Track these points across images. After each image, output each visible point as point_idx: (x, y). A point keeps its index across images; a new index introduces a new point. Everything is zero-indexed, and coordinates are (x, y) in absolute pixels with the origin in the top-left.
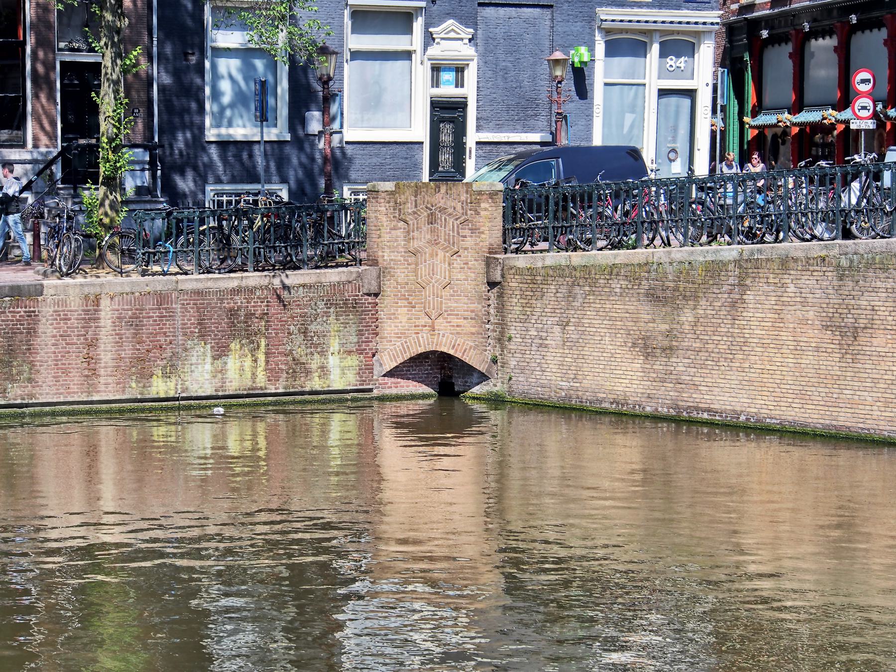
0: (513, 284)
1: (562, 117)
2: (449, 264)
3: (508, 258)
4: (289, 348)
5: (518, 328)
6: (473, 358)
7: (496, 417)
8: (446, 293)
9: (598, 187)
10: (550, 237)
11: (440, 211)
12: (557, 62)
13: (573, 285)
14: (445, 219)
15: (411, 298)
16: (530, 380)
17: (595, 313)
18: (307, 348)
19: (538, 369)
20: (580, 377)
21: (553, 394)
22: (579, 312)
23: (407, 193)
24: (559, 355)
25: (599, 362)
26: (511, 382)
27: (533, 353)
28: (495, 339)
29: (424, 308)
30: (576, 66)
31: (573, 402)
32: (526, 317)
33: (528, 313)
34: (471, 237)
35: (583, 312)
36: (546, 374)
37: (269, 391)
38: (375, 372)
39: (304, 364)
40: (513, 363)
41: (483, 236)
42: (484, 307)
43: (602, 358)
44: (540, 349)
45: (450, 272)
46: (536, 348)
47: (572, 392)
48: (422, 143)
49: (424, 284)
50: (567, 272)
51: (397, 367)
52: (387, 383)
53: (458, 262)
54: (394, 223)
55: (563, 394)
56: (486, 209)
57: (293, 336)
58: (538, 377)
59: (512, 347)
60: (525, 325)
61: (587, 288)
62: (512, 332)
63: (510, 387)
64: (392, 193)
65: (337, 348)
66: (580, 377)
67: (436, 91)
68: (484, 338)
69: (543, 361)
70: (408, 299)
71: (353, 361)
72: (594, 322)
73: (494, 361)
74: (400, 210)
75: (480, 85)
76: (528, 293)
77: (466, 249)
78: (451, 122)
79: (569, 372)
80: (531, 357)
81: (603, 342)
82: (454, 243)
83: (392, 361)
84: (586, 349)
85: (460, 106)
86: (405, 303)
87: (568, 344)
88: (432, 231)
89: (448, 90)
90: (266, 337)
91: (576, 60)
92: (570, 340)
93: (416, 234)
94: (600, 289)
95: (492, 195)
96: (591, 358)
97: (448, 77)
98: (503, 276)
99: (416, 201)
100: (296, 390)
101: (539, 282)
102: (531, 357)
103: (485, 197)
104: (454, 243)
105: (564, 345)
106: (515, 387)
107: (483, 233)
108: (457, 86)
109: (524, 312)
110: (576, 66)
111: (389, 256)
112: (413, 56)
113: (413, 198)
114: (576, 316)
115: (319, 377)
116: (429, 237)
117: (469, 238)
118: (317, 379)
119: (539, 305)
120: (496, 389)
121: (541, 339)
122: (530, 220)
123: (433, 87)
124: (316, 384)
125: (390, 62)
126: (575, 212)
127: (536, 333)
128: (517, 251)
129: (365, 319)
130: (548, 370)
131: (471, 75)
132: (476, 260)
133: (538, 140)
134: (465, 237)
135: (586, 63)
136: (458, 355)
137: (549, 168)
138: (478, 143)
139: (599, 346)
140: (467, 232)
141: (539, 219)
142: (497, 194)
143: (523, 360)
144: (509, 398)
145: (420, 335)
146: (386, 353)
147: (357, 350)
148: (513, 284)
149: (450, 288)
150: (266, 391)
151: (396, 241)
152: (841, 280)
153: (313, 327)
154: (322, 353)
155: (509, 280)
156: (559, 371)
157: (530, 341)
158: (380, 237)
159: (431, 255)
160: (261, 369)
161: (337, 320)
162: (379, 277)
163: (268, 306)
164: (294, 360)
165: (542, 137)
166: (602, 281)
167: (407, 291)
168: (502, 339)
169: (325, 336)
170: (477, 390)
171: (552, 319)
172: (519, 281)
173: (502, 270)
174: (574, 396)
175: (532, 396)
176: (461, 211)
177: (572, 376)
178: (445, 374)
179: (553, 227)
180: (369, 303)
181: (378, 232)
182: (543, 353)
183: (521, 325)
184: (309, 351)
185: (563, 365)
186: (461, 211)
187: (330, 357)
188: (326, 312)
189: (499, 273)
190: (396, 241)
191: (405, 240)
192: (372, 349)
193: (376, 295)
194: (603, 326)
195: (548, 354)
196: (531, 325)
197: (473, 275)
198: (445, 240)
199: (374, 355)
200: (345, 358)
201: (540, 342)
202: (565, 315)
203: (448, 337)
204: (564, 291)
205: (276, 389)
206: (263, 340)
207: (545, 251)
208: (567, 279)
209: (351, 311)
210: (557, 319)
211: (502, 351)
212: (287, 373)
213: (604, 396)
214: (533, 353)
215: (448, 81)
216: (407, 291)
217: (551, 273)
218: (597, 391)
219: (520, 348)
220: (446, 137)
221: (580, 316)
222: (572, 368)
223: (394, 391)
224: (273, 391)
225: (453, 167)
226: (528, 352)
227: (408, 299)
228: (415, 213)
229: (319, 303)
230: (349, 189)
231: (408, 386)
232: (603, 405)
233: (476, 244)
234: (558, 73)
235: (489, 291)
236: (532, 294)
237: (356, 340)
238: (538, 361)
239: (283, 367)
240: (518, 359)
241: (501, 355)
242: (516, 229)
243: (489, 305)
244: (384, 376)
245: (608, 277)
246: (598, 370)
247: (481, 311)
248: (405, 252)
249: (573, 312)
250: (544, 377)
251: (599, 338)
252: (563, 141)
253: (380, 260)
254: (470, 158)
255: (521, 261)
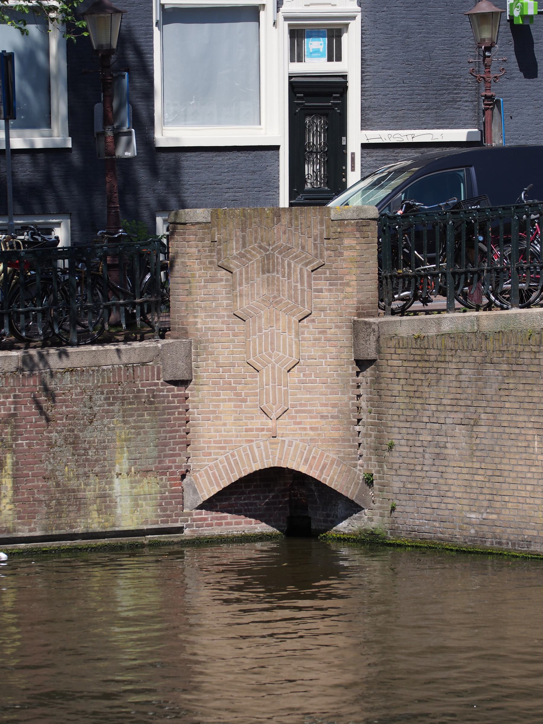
0: (395, 363)
1: (492, 102)
2: (297, 334)
3: (386, 322)
4: (50, 467)
6: (331, 477)
7: (373, 570)
8: (295, 376)
9: (520, 207)
10: (449, 288)
11: (280, 253)
12: (484, 17)
13: (484, 362)
14: (289, 265)
15: (239, 387)
16: (423, 510)
17: (517, 405)
18: (79, 466)
19: (434, 493)
20: (498, 505)
21: (457, 532)
22: (493, 404)
23: (231, 226)
24: (465, 470)
25: (524, 481)
26: (395, 514)
27: (426, 468)
29: (261, 402)
30: (515, 22)
31: (488, 544)
32: (415, 413)
33: (418, 407)
34: (330, 290)
35: (500, 404)
36: (446, 500)
37: (20, 534)
38: (187, 503)
39: (74, 491)
40: (396, 485)
43: (529, 475)
44: (437, 462)
45: (298, 345)
46: (430, 462)
47: (486, 528)
49: (258, 366)
50: (474, 342)
52: (205, 519)
53: (310, 329)
55: (473, 531)
56: (351, 248)
57: (56, 449)
58: (435, 505)
59: (391, 460)
60: (414, 425)
61: (505, 367)
62: (395, 436)
65: (125, 467)
66: (498, 505)
67: (298, 68)
68: (351, 447)
69: (441, 481)
70: (235, 389)
71: (150, 486)
72: (515, 418)
73: (369, 481)
74: (219, 253)
75: (367, 56)
77: (323, 310)
78: (322, 115)
79: (481, 497)
80: (423, 474)
81: (531, 450)
82: (303, 301)
83: (211, 484)
84: (505, 461)
85: (337, 87)
86: (230, 394)
87: (478, 453)
89: (316, 63)
90: (14, 452)
91: (516, 13)
92: (480, 447)
94: (525, 368)
95: (362, 223)
96: (513, 475)
97: (316, 45)
98: (378, 351)
99: (244, 237)
100: (63, 532)
101: (432, 358)
102: (423, 474)
103: (349, 228)
104: (303, 301)
105: (472, 455)
106: (400, 521)
107: (348, 284)
108: (330, 59)
109: (411, 406)
110: (515, 22)
111: (204, 323)
112: (262, 14)
113: (239, 233)
114: (488, 410)
115: (99, 511)
116: (265, 292)
117: (326, 294)
118: (95, 514)
119: (434, 394)
120: (373, 524)
121: (437, 446)
123: (292, 60)
124: (94, 522)
125: (207, 26)
126: (485, 249)
127: (429, 438)
128: (403, 311)
129: (169, 420)
130: (449, 494)
131: (352, 42)
132: (337, 327)
133: (464, 139)
134: (321, 291)
135: (530, 17)
136: (314, 473)
137: (456, 180)
138: (364, 146)
139: (524, 456)
140: (323, 285)
141: (431, 261)
143: (411, 479)
144: (391, 539)
145: (254, 444)
146: (202, 471)
147: (156, 468)
148: (395, 363)
149: (300, 371)
150: (15, 535)
152: (160, 330)
153: (87, 435)
154: (105, 475)
156: (465, 495)
157: (421, 450)
160: (6, 500)
161: (125, 422)
163: (15, 403)
164: (58, 485)
165: (469, 134)
166: (526, 355)
167: (234, 376)
168: (382, 448)
169: (105, 448)
170: (344, 527)
171: (452, 415)
172: (403, 357)
173: (378, 341)
174: (489, 535)
175: (426, 535)
177: (485, 504)
178: (287, 501)
179: (454, 274)
180: (174, 396)
181: (187, 287)
182: (441, 469)
183: (408, 425)
184: (81, 471)
185: (471, 487)
187: (116, 481)
188: (108, 411)
189: (373, 345)
190: (215, 299)
191: (228, 298)
192: (180, 467)
193: (184, 383)
194: (530, 425)
195: (450, 470)
196: (422, 425)
197: (333, 349)
198: (290, 297)
199: (183, 476)
200: (139, 482)
201: (437, 450)
202: (472, 409)
203: (297, 446)
204: (470, 372)
205: (30, 531)
206: (8, 455)
207: (444, 310)
208: (475, 353)
209: (146, 409)
210: (461, 415)
211: (381, 466)
212: (48, 506)
213: (535, 533)
215: (317, 51)
216: (234, 376)
217: (450, 344)
218: (523, 525)
219: (407, 460)
220: (315, 139)
221: (496, 411)
222: (485, 491)
223: (216, 531)
224: (27, 534)
226: (418, 468)
227: (235, 389)
228: (242, 256)
229: (95, 397)
230: (165, 221)
231: (240, 523)
232: (532, 548)
234: (486, 35)
235: (358, 374)
237: (155, 454)
238: (434, 480)
239: (41, 497)
241: (378, 472)
242: (398, 277)
243: (359, 396)
244: (201, 507)
245: (535, 349)
246: (523, 494)
248: (229, 317)
249: (484, 404)
250: (443, 506)
251: (524, 444)
252: (497, 141)
254: (353, 169)
255: (405, 326)
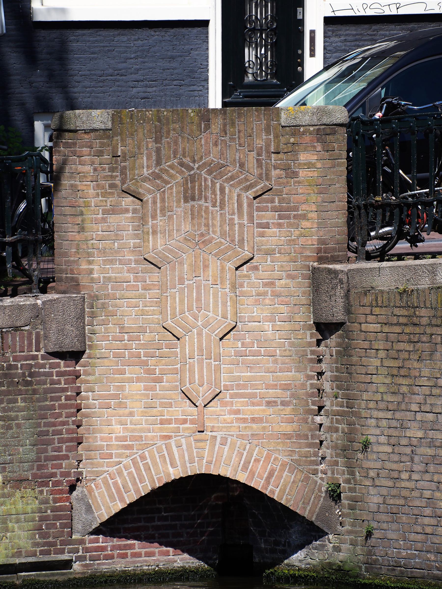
2: (234, 287)
3: (358, 270)
5: (384, 423)
11: (210, 172)
14: (222, 190)
15: (152, 361)
16: (413, 536)
19: (428, 511)
26: (372, 541)
27: (415, 476)
28: (335, 447)
29: (182, 381)
32: (399, 398)
33: (404, 389)
34: (280, 226)
38: (78, 525)
41: (305, 224)
42: (310, 378)
45: (235, 303)
48: (205, 24)
49: (179, 331)
51: (123, 511)
52: (103, 549)
53: (252, 281)
54: (110, 200)
56: (310, 165)
58: (429, 530)
59: (371, 464)
60: (398, 415)
63: (370, 553)
64: (105, 133)
68: (310, 445)
73: (335, 495)
74: (123, 172)
76: (401, 346)
82: (241, 241)
88: (194, 215)
93: (160, 221)
98: (348, 310)
99: (158, 151)
101: (425, 321)
103: (307, 138)
106: (380, 551)
107: (304, 217)
120: (342, 556)
122: (405, 186)
127: (420, 434)
132: (289, 277)
134: (267, 226)
142: (334, 133)
143: (394, 492)
145: (172, 442)
146: (99, 480)
147: (35, 476)
151: (117, 238)
155: (362, 319)
157: (408, 450)
158: (82, 229)
159: (194, 268)
162: (81, 317)
167: (144, 346)
172: (382, 319)
173: (347, 296)
176: (256, 172)
180: (60, 374)
183: (389, 415)
186: (256, 172)
189: (340, 302)
190: (117, 238)
191: (136, 236)
192: (68, 474)
193: (76, 356)
196: (409, 415)
198: (223, 235)
199: (72, 488)
200: (10, 496)
201: (430, 451)
203: (233, 444)
211: (352, 473)
214: (415, 476)
225: (274, 76)
226: (405, 476)
227: (146, 363)
228: (157, 176)
231: (152, 554)
233: (291, 242)
235: (319, 343)
236: (410, 347)
237: (33, 456)
238: (427, 494)
240: (384, 491)
241: (348, 481)
243: (320, 374)
244: (96, 532)
247: (303, 386)
248: (137, 262)
253: (84, 281)
255: (385, 276)
